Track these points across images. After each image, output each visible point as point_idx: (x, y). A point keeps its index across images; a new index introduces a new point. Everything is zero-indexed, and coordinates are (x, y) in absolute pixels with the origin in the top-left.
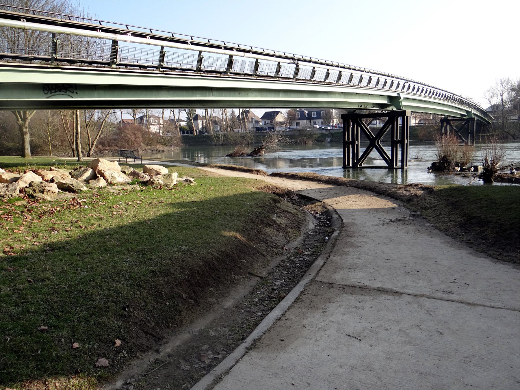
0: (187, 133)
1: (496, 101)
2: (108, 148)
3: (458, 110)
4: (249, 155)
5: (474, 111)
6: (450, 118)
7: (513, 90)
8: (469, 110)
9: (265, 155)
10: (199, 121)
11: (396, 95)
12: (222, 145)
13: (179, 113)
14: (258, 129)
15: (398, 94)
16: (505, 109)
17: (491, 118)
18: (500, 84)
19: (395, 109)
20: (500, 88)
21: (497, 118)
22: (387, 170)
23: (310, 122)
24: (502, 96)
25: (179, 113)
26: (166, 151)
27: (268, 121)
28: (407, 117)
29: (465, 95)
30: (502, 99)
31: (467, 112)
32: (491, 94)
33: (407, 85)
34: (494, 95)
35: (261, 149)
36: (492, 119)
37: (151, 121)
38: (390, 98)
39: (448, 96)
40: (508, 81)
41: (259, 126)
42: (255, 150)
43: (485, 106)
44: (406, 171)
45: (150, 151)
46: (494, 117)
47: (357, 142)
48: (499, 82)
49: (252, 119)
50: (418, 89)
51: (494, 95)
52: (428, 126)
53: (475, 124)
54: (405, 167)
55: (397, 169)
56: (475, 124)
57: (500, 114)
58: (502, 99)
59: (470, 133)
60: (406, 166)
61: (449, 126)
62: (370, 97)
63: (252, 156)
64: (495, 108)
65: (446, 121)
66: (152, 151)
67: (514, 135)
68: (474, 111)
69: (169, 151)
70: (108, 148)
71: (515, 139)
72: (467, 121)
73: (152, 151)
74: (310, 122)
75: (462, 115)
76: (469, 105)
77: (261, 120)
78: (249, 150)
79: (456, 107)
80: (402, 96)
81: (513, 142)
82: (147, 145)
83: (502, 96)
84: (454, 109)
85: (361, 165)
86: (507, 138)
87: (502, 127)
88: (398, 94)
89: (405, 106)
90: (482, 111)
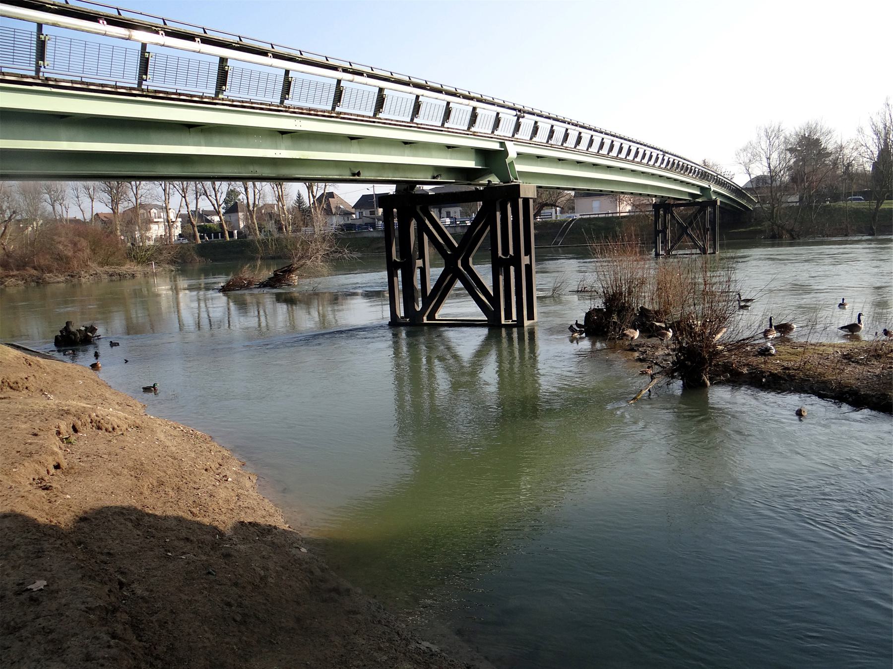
0: (216, 236)
1: (760, 169)
2: (15, 273)
3: (681, 187)
4: (263, 285)
5: (714, 188)
6: (672, 202)
7: (791, 150)
8: (705, 184)
9: (298, 283)
10: (240, 214)
11: (495, 146)
12: (273, 258)
13: (197, 199)
14: (349, 227)
15: (502, 144)
16: (774, 184)
17: (750, 200)
18: (765, 138)
19: (495, 180)
20: (764, 144)
21: (763, 200)
22: (484, 331)
23: (440, 212)
24: (769, 159)
25: (197, 199)
26: (139, 276)
27: (366, 213)
28: (526, 201)
29: (695, 156)
30: (769, 164)
31: (702, 189)
32: (749, 155)
33: (666, 159)
34: (755, 156)
35: (289, 270)
36: (753, 204)
37: (153, 215)
38: (482, 153)
39: (673, 163)
40: (779, 131)
41: (350, 222)
42: (276, 275)
43: (741, 180)
44: (532, 333)
45: (106, 276)
46: (757, 197)
47: (419, 263)
48: (763, 134)
49: (338, 208)
50: (637, 153)
51: (755, 156)
52: (639, 216)
53: (717, 212)
54: (527, 323)
55: (509, 327)
56: (717, 212)
57: (766, 193)
58: (769, 164)
59: (708, 230)
60: (531, 317)
61: (669, 217)
62: (435, 150)
63: (273, 287)
64: (759, 181)
65: (664, 205)
66: (111, 275)
67: (792, 230)
68: (714, 188)
69: (145, 275)
70: (15, 273)
71: (794, 239)
72: (703, 205)
73: (111, 275)
74: (440, 212)
75: (691, 195)
76: (704, 176)
77: (353, 211)
78: (266, 274)
79: (688, 183)
80: (513, 150)
81: (791, 245)
82: (102, 264)
83: (769, 159)
84: (682, 186)
85: (431, 317)
86: (781, 237)
87: (771, 216)
88: (502, 144)
89: (523, 174)
90: (737, 190)
